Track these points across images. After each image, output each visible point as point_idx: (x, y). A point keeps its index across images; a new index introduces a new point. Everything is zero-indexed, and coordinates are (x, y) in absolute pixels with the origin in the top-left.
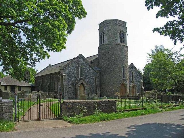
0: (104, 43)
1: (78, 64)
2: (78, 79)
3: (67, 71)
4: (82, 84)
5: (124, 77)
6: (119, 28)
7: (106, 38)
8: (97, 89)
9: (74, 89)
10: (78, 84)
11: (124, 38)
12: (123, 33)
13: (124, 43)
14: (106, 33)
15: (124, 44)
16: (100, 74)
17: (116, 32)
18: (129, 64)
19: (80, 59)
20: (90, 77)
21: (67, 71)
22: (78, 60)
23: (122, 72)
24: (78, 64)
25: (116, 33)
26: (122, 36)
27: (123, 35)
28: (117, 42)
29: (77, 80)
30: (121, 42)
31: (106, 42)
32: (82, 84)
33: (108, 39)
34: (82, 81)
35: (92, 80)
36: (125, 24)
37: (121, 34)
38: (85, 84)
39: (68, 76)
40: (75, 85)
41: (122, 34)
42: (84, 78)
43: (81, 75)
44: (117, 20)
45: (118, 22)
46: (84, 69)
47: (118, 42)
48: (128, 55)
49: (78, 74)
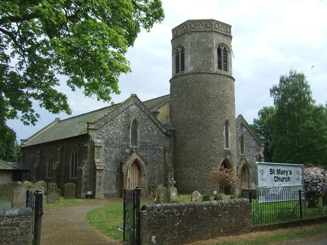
0: (183, 69)
2: (127, 151)
5: (227, 146)
7: (188, 59)
11: (226, 61)
13: (226, 69)
14: (188, 48)
17: (210, 46)
19: (132, 105)
24: (128, 116)
25: (210, 50)
28: (211, 69)
29: (124, 153)
30: (220, 67)
31: (189, 68)
33: (192, 63)
34: (135, 156)
40: (120, 165)
42: (141, 148)
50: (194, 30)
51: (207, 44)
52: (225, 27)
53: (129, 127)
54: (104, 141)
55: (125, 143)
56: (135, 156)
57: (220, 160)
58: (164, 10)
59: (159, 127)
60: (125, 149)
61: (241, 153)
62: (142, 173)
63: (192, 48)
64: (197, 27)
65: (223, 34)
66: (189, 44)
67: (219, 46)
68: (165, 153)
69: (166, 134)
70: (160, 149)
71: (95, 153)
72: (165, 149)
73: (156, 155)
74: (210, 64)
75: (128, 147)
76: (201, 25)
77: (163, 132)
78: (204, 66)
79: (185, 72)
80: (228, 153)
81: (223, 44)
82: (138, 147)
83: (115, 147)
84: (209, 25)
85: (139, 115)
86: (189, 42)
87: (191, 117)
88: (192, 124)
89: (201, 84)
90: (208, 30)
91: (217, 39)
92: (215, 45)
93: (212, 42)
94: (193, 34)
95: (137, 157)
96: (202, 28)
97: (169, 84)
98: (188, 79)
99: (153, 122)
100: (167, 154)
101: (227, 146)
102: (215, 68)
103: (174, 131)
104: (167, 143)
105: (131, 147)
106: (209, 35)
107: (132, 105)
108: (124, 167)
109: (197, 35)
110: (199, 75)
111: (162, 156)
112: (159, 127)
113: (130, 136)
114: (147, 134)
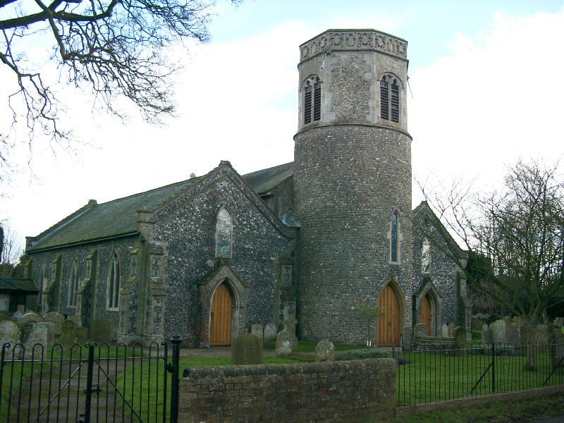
0: (317, 117)
5: (394, 259)
6: (376, 65)
7: (326, 102)
11: (396, 100)
12: (395, 81)
13: (396, 118)
17: (367, 76)
20: (260, 253)
27: (396, 88)
29: (205, 267)
30: (384, 115)
31: (327, 117)
32: (226, 283)
33: (335, 104)
35: (266, 269)
38: (237, 285)
40: (196, 286)
41: (390, 87)
51: (361, 73)
55: (206, 249)
59: (270, 221)
60: (206, 260)
62: (238, 303)
65: (392, 56)
67: (384, 77)
68: (281, 268)
70: (271, 261)
80: (397, 269)
81: (391, 74)
83: (188, 256)
84: (365, 39)
85: (235, 198)
88: (331, 217)
90: (363, 47)
94: (337, 54)
99: (260, 211)
102: (375, 116)
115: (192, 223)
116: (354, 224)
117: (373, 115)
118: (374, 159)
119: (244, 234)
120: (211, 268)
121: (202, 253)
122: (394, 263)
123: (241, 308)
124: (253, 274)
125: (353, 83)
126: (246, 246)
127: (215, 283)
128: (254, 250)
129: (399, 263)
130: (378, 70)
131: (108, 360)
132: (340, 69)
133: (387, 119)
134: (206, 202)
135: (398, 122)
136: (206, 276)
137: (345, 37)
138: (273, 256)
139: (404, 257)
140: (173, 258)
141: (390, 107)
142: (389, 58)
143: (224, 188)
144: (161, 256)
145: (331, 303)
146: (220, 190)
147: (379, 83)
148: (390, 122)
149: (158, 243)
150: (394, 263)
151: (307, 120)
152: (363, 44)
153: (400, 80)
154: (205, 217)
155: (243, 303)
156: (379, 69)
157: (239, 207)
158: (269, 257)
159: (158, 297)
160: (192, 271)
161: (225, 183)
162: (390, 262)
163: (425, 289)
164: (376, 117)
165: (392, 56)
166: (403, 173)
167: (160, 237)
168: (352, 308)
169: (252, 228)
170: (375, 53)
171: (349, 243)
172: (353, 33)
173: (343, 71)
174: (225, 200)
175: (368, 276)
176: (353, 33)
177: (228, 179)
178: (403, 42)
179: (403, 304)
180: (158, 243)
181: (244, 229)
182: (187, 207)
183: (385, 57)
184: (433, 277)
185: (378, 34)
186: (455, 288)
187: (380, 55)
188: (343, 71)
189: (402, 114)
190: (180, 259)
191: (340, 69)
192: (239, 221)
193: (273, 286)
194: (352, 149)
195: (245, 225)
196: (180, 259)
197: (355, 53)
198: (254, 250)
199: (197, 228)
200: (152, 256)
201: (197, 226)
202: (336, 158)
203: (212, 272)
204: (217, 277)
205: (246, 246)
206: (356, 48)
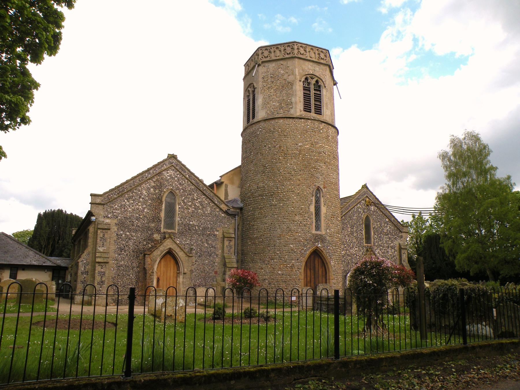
0: (254, 117)
1: (160, 186)
2: (157, 236)
3: (116, 209)
4: (170, 253)
5: (318, 228)
6: (299, 70)
7: (259, 101)
8: (224, 274)
9: (139, 272)
10: (155, 253)
11: (318, 98)
12: (317, 82)
13: (319, 110)
14: (259, 85)
15: (318, 117)
16: (243, 221)
17: (291, 78)
18: (348, 188)
19: (166, 170)
20: (204, 229)
21: (116, 209)
22: (160, 174)
23: (312, 209)
24: (160, 186)
25: (291, 84)
26: (313, 92)
27: (318, 87)
28: (292, 111)
29: (150, 239)
30: (307, 108)
31: (261, 114)
32: (170, 253)
33: (265, 104)
34: (168, 244)
35: (210, 242)
36: (322, 56)
37: (309, 84)
38: (181, 255)
39: (121, 225)
40: (142, 255)
41: (312, 87)
42: (181, 233)
43: (170, 224)
44: (337, 142)
45: (298, 49)
46: (179, 204)
47: (296, 111)
48: (340, 166)
49: (156, 219)
50: (268, 59)
51: (285, 77)
52: (317, 52)
53: (161, 201)
54: (115, 221)
55: (153, 225)
56: (168, 244)
57: (305, 251)
58: (63, 40)
59: (214, 203)
60: (153, 234)
61: (367, 243)
62: (181, 270)
63: (265, 84)
64: (272, 55)
65: (313, 61)
66: (260, 80)
67: (306, 79)
68: (224, 240)
69: (226, 212)
70: (215, 235)
71: (99, 239)
72: (223, 234)
73: (208, 244)
74: (290, 104)
75: (158, 231)
76: (278, 52)
77: (221, 209)
78: (281, 108)
79: (255, 120)
80: (322, 238)
81: (312, 76)
82: (176, 232)
83: (136, 231)
84: (289, 50)
85: (180, 184)
86: (261, 76)
87: (261, 185)
88: (262, 195)
89: (276, 134)
90: (287, 56)
91: (299, 70)
92: (298, 77)
93: (293, 73)
94: (266, 64)
95: (171, 246)
96: (279, 55)
97: (241, 139)
98: (258, 129)
99: (204, 194)
100: (226, 243)
101: (318, 228)
102: (298, 109)
103: (241, 209)
104: (229, 226)
105: (162, 230)
106: (290, 63)
107: (166, 170)
108: (148, 260)
109: (272, 65)
110: (273, 122)
111: (219, 245)
112: (214, 203)
113: (163, 215)
114: (193, 212)
115: (140, 204)
116: (280, 200)
117: (296, 108)
118: (297, 145)
119: (188, 213)
120: (158, 241)
121: (149, 229)
122: (318, 232)
123: (185, 274)
124: (197, 245)
125: (288, 92)
126: (191, 223)
127: (159, 253)
128: (199, 226)
129: (323, 232)
130: (299, 73)
131: (352, 333)
132: (269, 76)
133: (310, 112)
134: (154, 187)
135: (321, 114)
136: (152, 247)
137: (272, 50)
138: (218, 231)
139: (328, 227)
140: (121, 232)
141: (313, 102)
142: (311, 64)
143: (170, 176)
144: (109, 231)
145: (262, 269)
146: (166, 177)
147: (302, 83)
148: (313, 115)
149: (107, 221)
150: (318, 232)
151: (248, 121)
152: (287, 54)
153: (322, 80)
154: (152, 199)
155: (186, 270)
156: (301, 71)
157: (185, 191)
158: (213, 231)
159: (101, 264)
160: (140, 243)
161: (171, 172)
162: (314, 232)
163: (481, 285)
164: (298, 110)
165: (313, 61)
166: (329, 160)
167: (109, 216)
168: (279, 272)
169: (197, 208)
170: (296, 60)
171: (276, 216)
172: (279, 46)
173: (271, 77)
174: (172, 185)
175: (292, 244)
176: (279, 46)
177: (173, 168)
178: (324, 51)
179: (328, 268)
180: (107, 221)
181: (189, 209)
182: (135, 191)
183: (307, 63)
184: (376, 248)
185: (300, 45)
186: (398, 257)
187: (301, 61)
188: (271, 77)
189: (325, 107)
190: (128, 233)
191: (269, 76)
192: (184, 202)
193: (217, 255)
194: (278, 138)
195: (190, 206)
196: (128, 233)
197: (282, 62)
198: (199, 226)
199: (144, 208)
200: (99, 231)
201: (144, 206)
202: (265, 146)
203: (157, 244)
204: (161, 248)
205: (191, 223)
206: (281, 57)
